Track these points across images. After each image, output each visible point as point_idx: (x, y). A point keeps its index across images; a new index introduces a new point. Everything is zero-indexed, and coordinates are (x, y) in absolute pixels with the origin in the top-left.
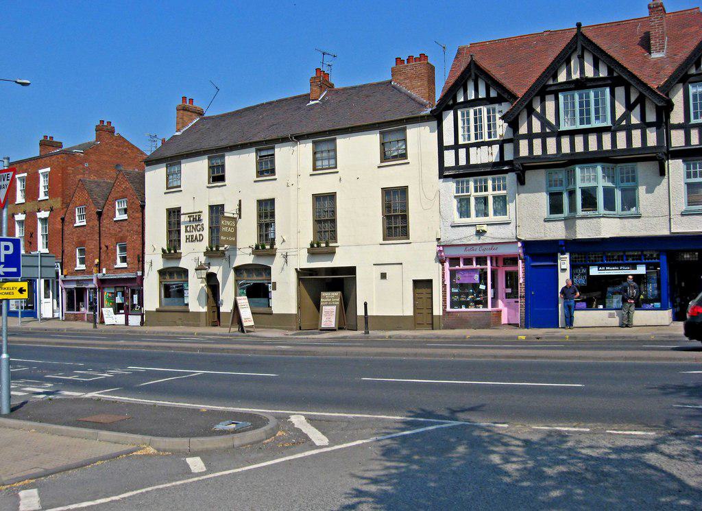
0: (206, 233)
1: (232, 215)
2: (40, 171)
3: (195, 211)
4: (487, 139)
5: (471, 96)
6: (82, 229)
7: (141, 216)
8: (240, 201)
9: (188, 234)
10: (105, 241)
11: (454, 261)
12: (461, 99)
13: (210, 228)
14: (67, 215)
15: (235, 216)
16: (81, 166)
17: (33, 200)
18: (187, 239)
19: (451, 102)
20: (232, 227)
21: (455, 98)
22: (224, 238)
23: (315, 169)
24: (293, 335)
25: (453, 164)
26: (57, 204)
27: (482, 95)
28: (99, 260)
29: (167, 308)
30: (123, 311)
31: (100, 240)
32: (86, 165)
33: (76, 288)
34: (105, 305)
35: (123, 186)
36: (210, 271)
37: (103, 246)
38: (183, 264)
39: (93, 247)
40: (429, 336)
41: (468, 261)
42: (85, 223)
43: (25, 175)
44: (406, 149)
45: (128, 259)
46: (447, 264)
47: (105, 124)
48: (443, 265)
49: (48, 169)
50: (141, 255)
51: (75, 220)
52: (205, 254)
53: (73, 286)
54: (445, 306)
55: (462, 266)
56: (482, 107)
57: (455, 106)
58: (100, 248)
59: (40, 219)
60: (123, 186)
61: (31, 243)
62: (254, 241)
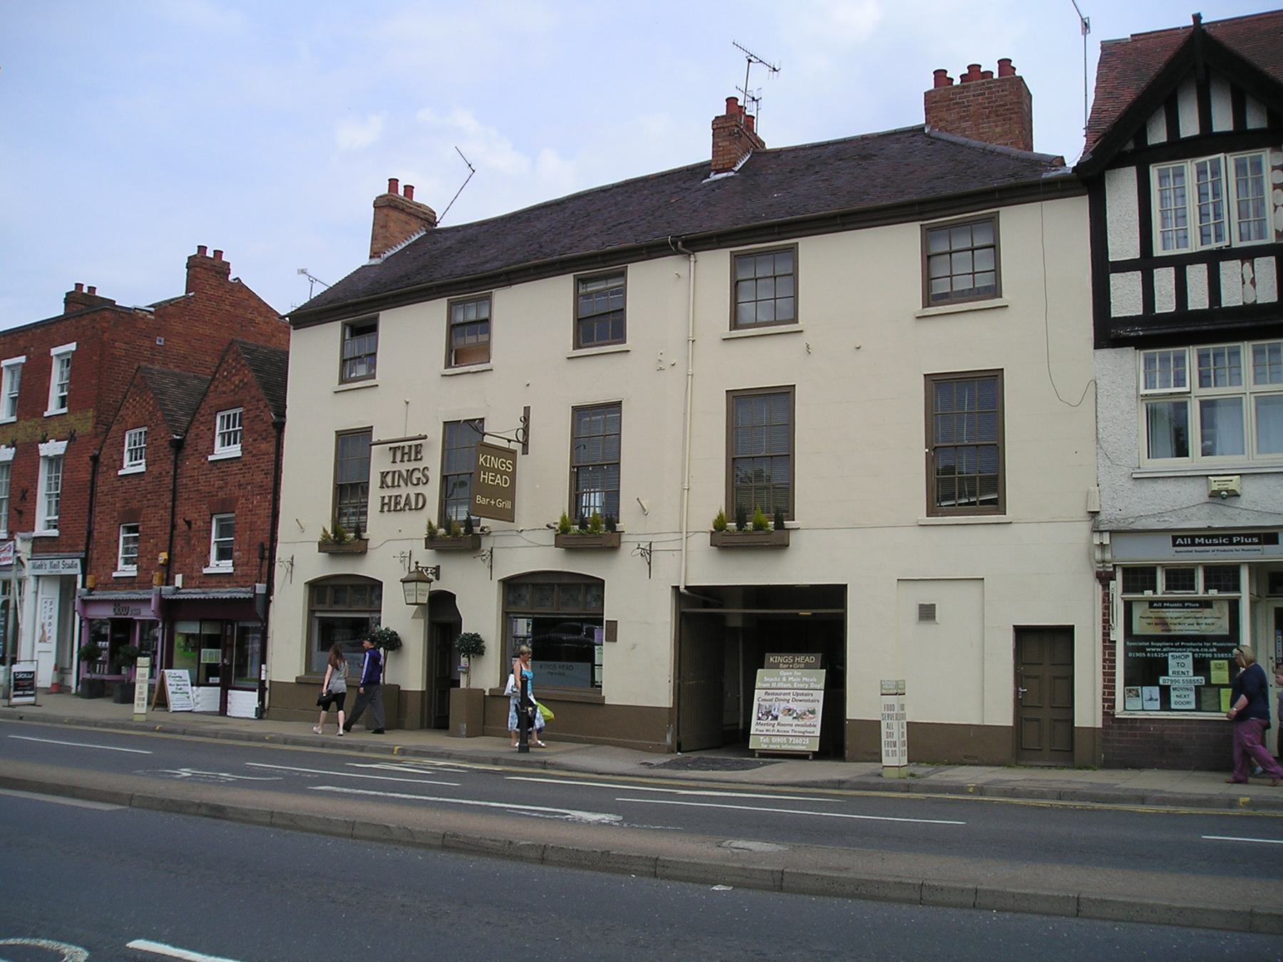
0: (432, 492)
1: (504, 444)
2: (54, 351)
3: (409, 435)
4: (1237, 244)
5: (1189, 126)
6: (135, 482)
7: (272, 450)
8: (527, 409)
9: (387, 493)
10: (187, 510)
11: (1138, 577)
12: (1189, 126)
13: (445, 479)
14: (104, 449)
15: (513, 446)
16: (147, 343)
17: (34, 416)
18: (383, 505)
19: (1130, 146)
20: (505, 473)
21: (1142, 135)
22: (485, 501)
23: (735, 325)
24: (665, 765)
25: (1139, 311)
26: (85, 424)
27: (1223, 122)
28: (169, 555)
29: (201, 666)
30: (217, 680)
31: (174, 507)
32: (160, 341)
33: (112, 620)
34: (176, 662)
35: (236, 380)
36: (436, 586)
37: (180, 522)
38: (367, 568)
39: (157, 523)
40: (481, 755)
41: (1180, 577)
42: (142, 468)
43: (22, 359)
44: (997, 271)
45: (236, 554)
46: (1117, 585)
47: (85, 290)
48: (1106, 586)
49: (72, 347)
50: (267, 545)
51: (122, 460)
52: (324, 546)
53: (107, 613)
54: (1109, 700)
55: (1200, 591)
56: (1221, 155)
57: (1143, 158)
58: (173, 527)
59: (45, 457)
60: (236, 380)
61: (20, 512)
62: (559, 507)
